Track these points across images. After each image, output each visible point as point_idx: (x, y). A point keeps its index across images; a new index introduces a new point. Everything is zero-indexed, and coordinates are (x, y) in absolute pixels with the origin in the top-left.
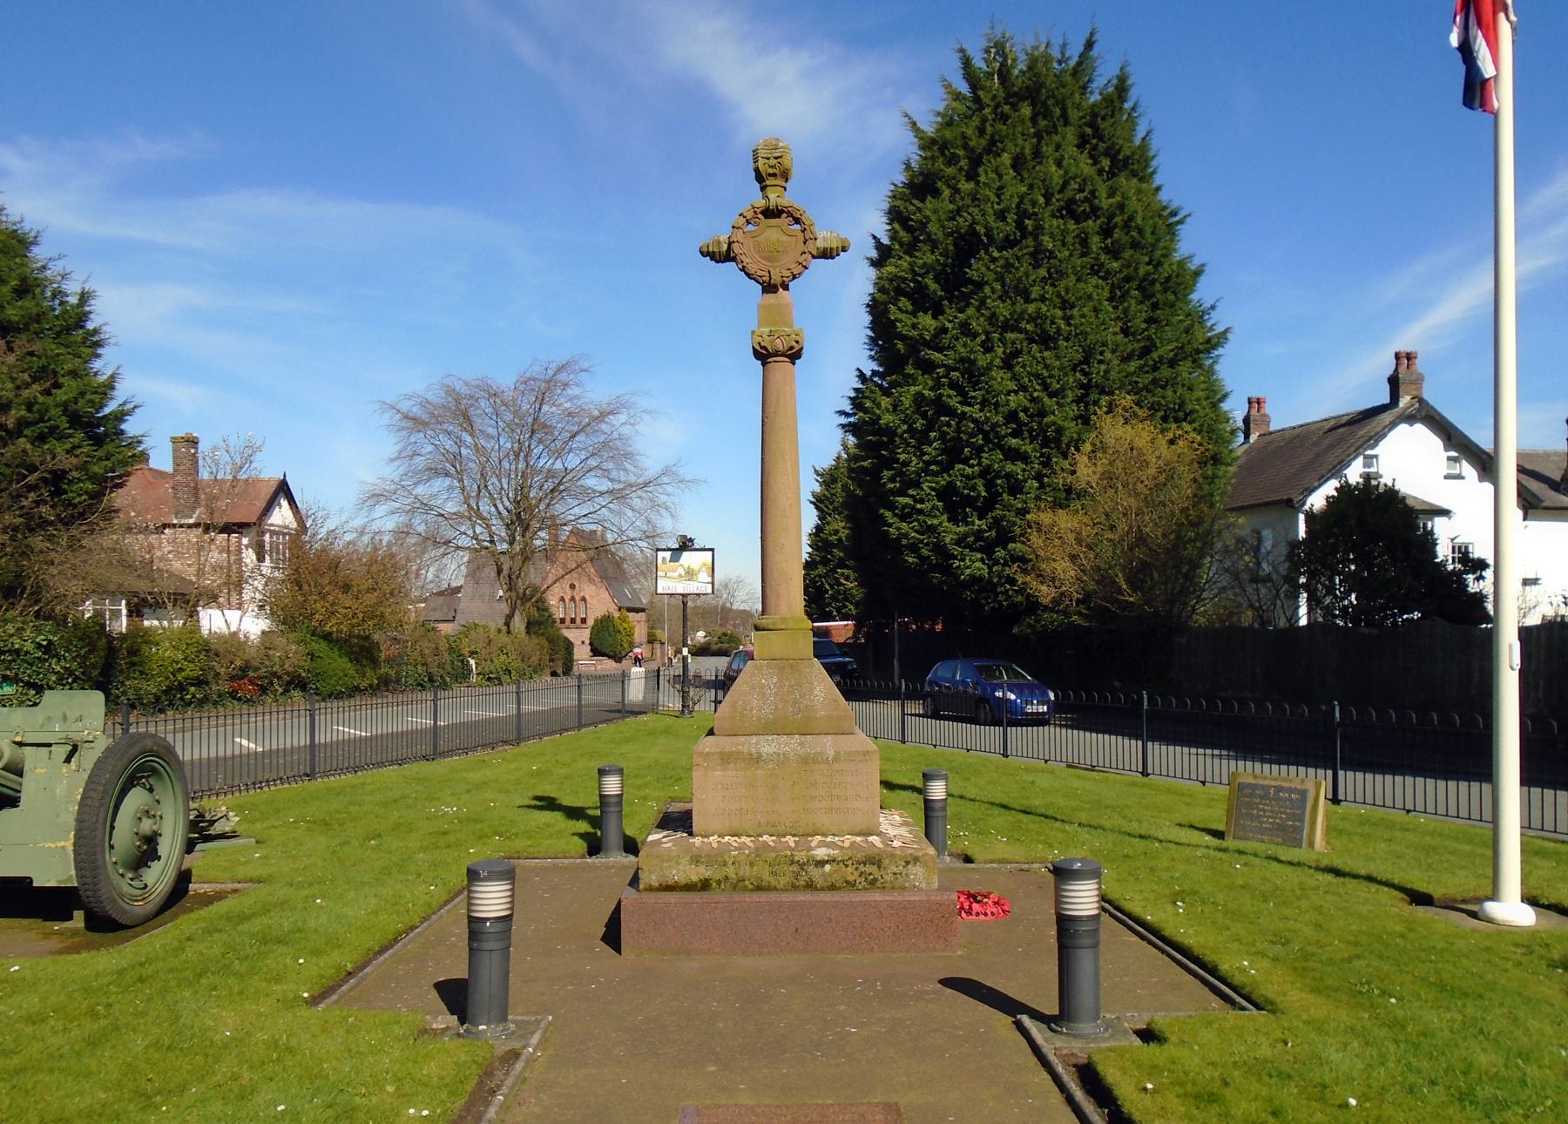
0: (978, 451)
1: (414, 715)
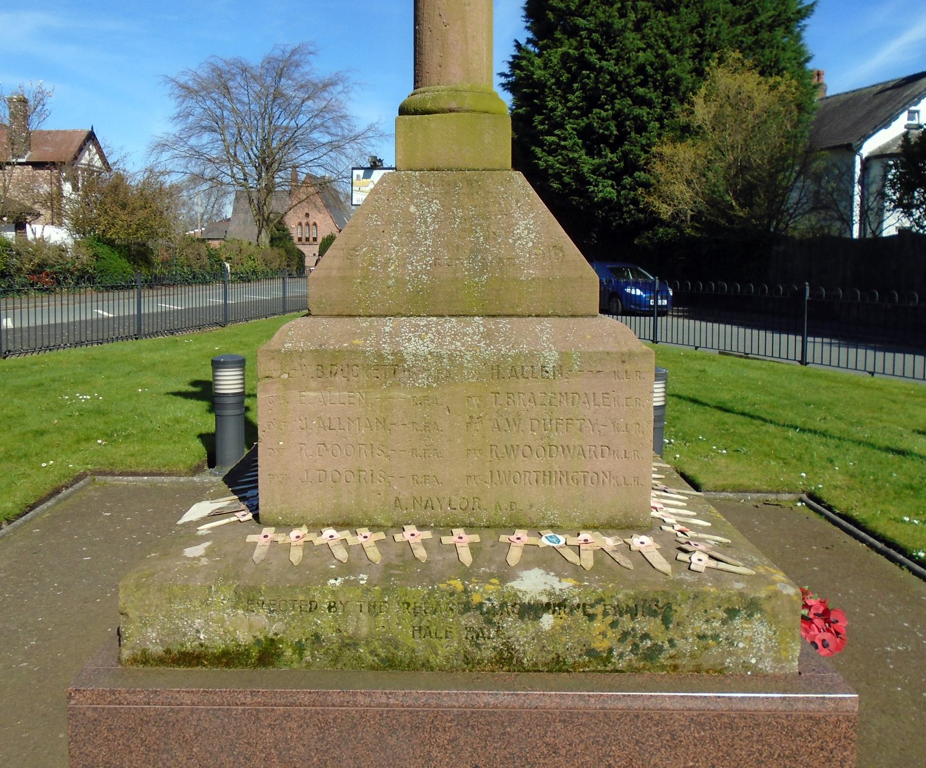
0: (612, 97)
1: (172, 303)
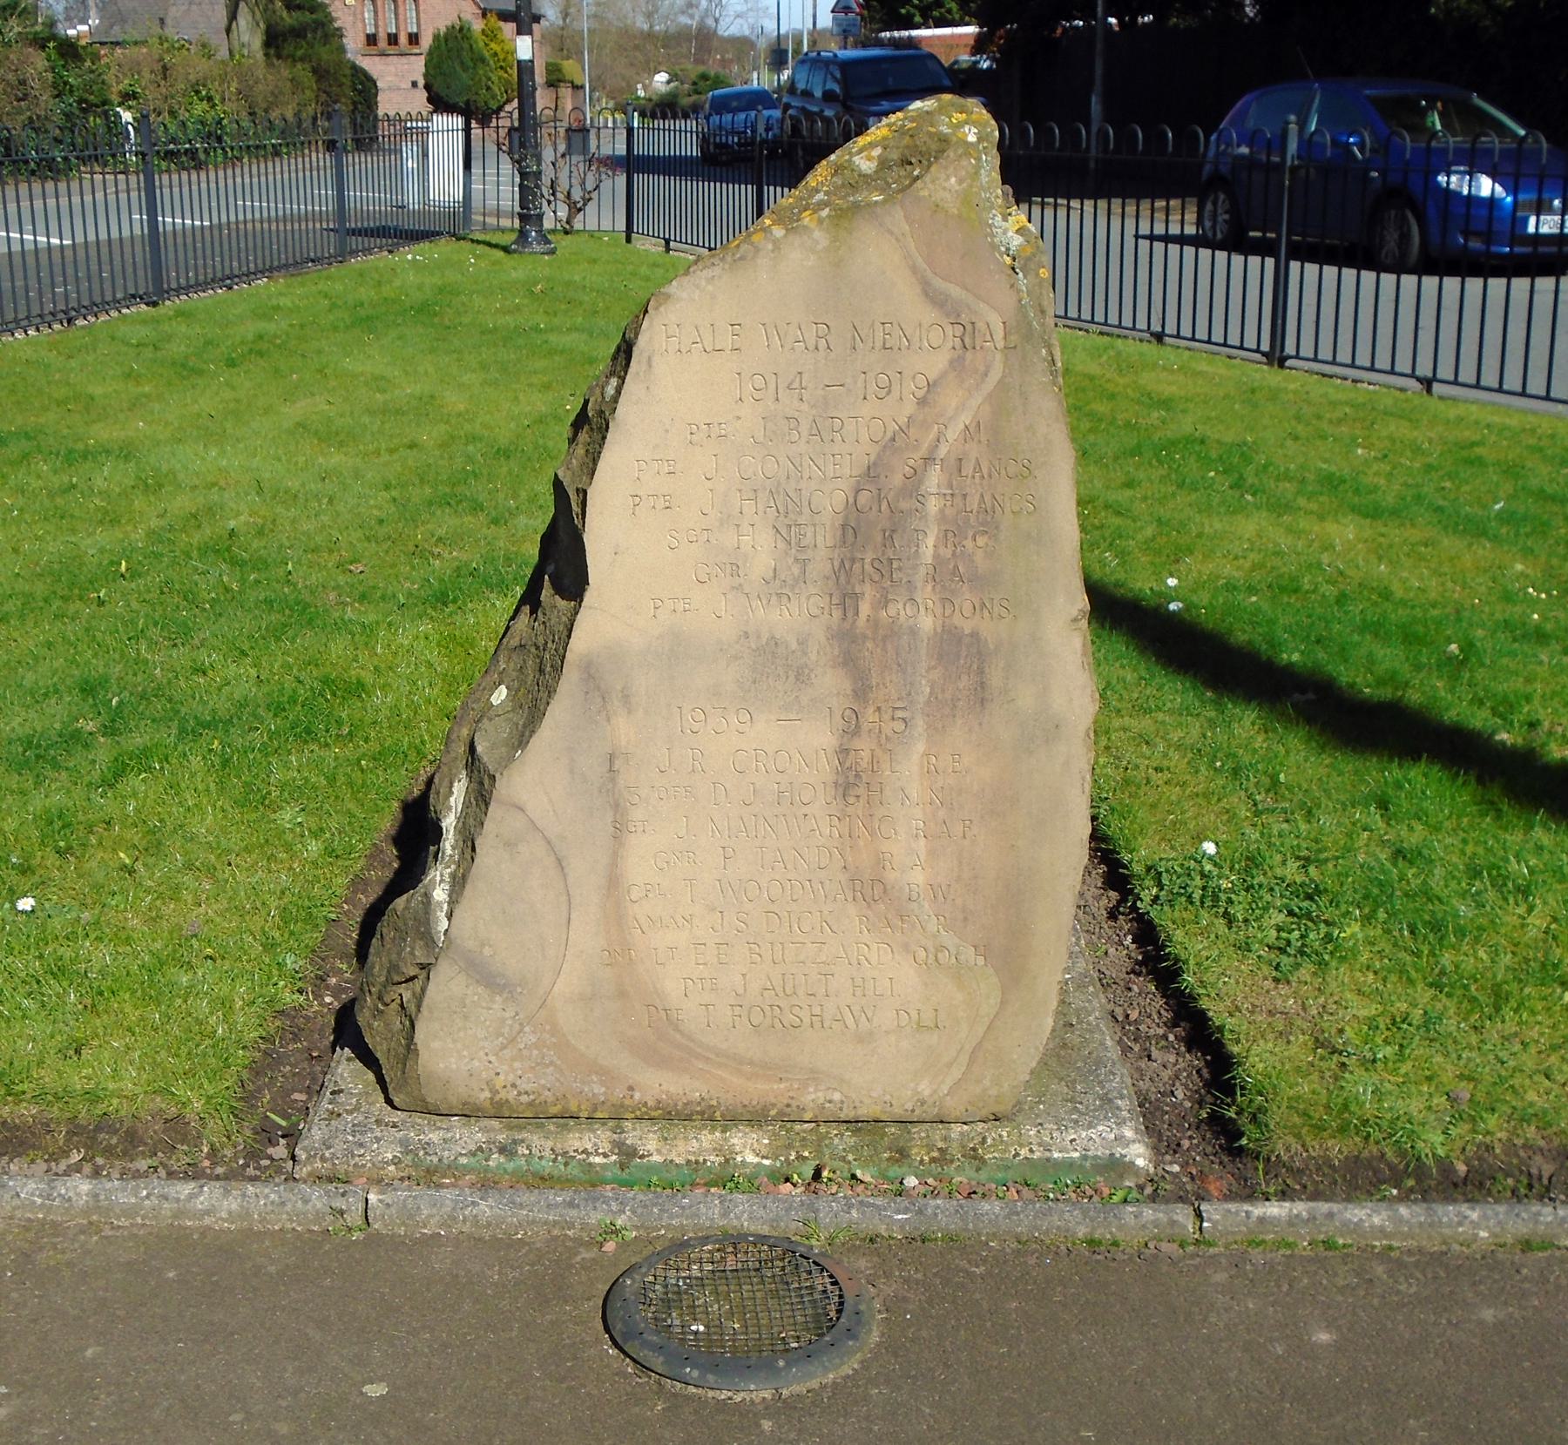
1: (41, 226)
